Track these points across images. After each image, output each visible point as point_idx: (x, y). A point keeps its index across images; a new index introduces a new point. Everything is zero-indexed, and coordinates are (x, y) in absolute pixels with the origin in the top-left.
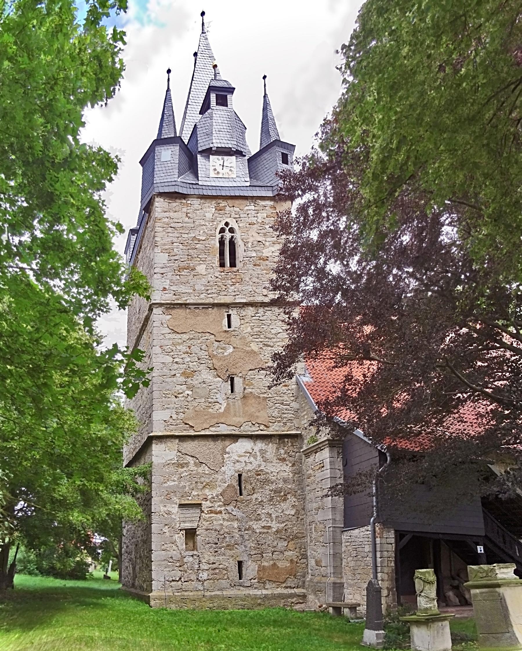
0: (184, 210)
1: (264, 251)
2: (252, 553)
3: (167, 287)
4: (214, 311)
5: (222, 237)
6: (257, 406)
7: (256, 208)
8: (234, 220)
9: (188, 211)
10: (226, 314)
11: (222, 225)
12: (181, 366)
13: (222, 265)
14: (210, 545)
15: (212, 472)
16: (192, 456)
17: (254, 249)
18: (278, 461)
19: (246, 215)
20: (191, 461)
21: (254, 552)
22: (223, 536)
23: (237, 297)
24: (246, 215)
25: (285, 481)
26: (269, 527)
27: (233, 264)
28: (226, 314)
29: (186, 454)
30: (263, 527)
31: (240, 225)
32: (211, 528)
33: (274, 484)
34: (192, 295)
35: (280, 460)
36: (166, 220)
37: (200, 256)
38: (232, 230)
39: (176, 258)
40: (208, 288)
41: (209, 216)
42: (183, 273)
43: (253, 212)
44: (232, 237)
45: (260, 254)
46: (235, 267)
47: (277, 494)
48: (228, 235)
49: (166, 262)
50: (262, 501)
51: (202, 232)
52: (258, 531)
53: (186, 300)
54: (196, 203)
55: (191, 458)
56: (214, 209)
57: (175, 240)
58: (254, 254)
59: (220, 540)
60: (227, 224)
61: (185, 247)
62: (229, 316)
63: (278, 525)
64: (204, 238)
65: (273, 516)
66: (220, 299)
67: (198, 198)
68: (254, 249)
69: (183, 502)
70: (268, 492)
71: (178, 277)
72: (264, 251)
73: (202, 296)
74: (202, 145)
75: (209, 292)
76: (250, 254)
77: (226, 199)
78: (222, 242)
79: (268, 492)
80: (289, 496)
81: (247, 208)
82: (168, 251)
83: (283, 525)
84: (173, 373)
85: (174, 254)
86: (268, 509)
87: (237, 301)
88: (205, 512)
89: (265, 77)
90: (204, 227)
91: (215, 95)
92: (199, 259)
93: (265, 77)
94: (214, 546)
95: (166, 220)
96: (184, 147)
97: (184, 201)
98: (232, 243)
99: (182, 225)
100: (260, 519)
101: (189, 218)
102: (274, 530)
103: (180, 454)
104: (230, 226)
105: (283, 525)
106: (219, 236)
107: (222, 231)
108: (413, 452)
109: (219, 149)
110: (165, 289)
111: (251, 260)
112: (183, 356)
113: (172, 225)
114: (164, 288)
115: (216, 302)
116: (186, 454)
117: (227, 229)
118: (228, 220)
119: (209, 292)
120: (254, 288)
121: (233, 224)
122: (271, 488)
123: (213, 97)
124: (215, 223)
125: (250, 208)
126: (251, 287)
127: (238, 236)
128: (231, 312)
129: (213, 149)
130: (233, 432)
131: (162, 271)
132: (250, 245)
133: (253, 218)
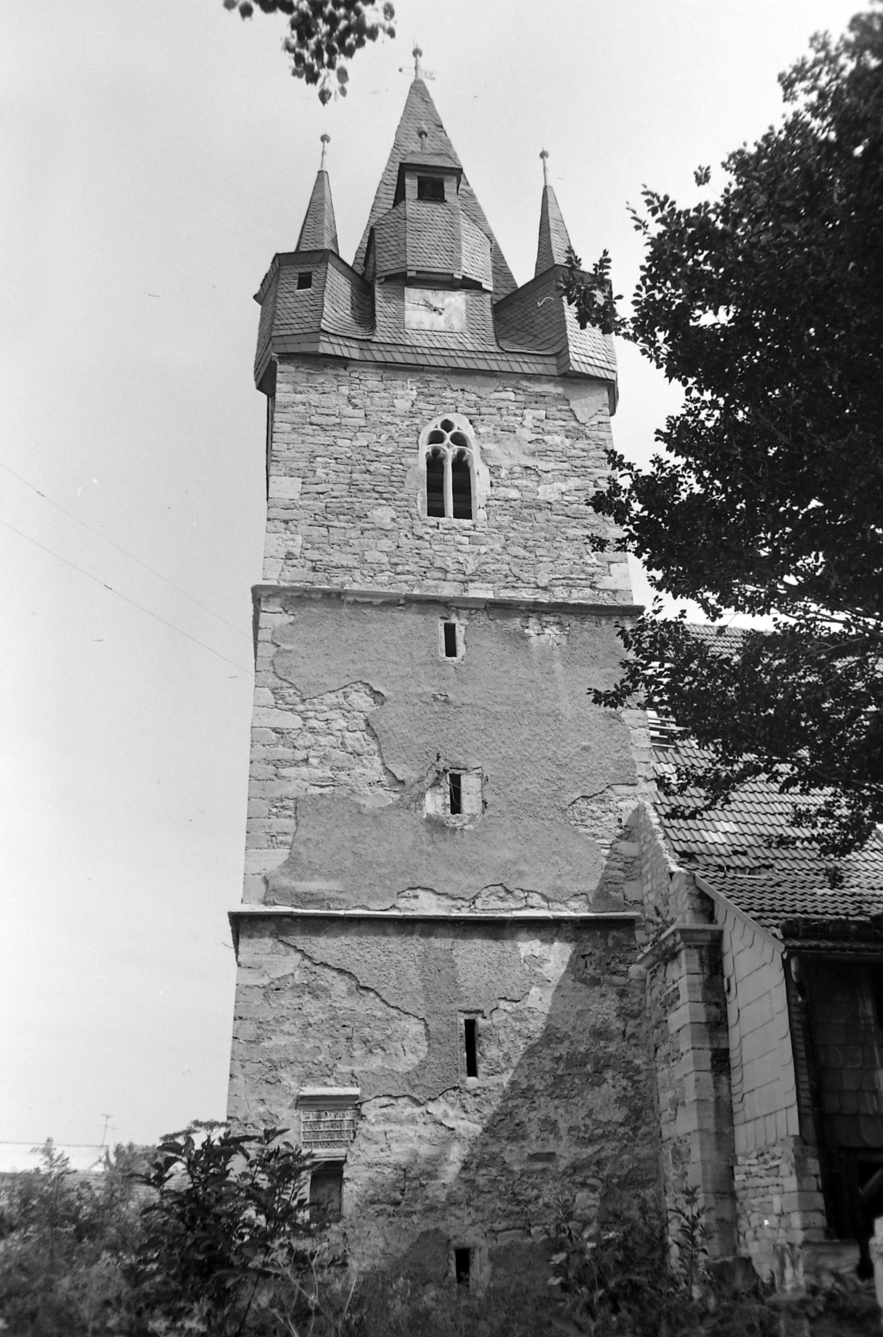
0: (345, 390)
1: (539, 489)
2: (497, 1226)
3: (297, 551)
4: (411, 619)
5: (436, 452)
6: (519, 846)
7: (519, 398)
8: (466, 420)
9: (353, 393)
10: (443, 622)
11: (435, 425)
12: (323, 740)
13: (436, 510)
14: (378, 1207)
15: (394, 1012)
16: (341, 971)
17: (516, 482)
18: (579, 985)
19: (494, 410)
20: (341, 985)
21: (504, 1224)
22: (415, 1184)
23: (471, 585)
24: (494, 410)
25: (599, 1034)
26: (550, 1157)
27: (464, 511)
28: (443, 622)
29: (326, 965)
30: (534, 1157)
31: (482, 430)
32: (385, 1161)
33: (567, 1043)
34: (357, 573)
35: (583, 981)
36: (301, 409)
37: (379, 489)
38: (459, 439)
39: (319, 488)
40: (395, 560)
41: (402, 405)
42: (336, 523)
43: (512, 406)
44: (461, 454)
45: (529, 496)
46: (470, 518)
47: (575, 1070)
48: (450, 451)
49: (297, 496)
50: (530, 1088)
51: (384, 437)
52: (516, 1168)
53: (343, 584)
54: (372, 381)
55: (339, 977)
56: (415, 393)
57: (320, 451)
58: (514, 494)
59: (408, 1195)
60: (447, 425)
61: (342, 467)
62: (450, 630)
63: (575, 1150)
64: (390, 450)
65: (563, 1126)
66: (428, 588)
67: (379, 367)
68: (516, 482)
69: (310, 1090)
70: (548, 1065)
71: (324, 531)
72: (539, 489)
73: (383, 578)
74: (386, 264)
75: (400, 569)
76: (502, 492)
77: (443, 373)
78: (435, 463)
79: (548, 1065)
80: (609, 1074)
81: (497, 395)
82: (301, 473)
83: (590, 1151)
84: (301, 755)
85: (314, 480)
86: (547, 1107)
87: (472, 594)
88: (369, 1117)
89: (543, 155)
90: (391, 428)
91: (415, 183)
92: (376, 495)
93: (543, 155)
94: (390, 1209)
95: (301, 409)
96: (348, 272)
97: (342, 372)
98: (462, 467)
99: (338, 420)
100: (524, 1138)
101: (355, 406)
102: (563, 1164)
103: (307, 963)
104: (455, 430)
105: (590, 1151)
106: (426, 449)
107: (436, 438)
108: (322, 221)
109: (420, 275)
110: (289, 556)
111: (507, 506)
112: (328, 715)
113: (314, 419)
114: (289, 553)
115: (416, 592)
116: (326, 965)
117: (448, 435)
118: (450, 417)
119: (400, 569)
120: (516, 570)
121: (462, 425)
122: (557, 1054)
123: (411, 184)
124: (417, 421)
125: (504, 395)
126: (506, 567)
127: (473, 452)
128: (454, 620)
129: (410, 274)
130: (455, 913)
131: (286, 515)
132: (503, 473)
133: (512, 418)
